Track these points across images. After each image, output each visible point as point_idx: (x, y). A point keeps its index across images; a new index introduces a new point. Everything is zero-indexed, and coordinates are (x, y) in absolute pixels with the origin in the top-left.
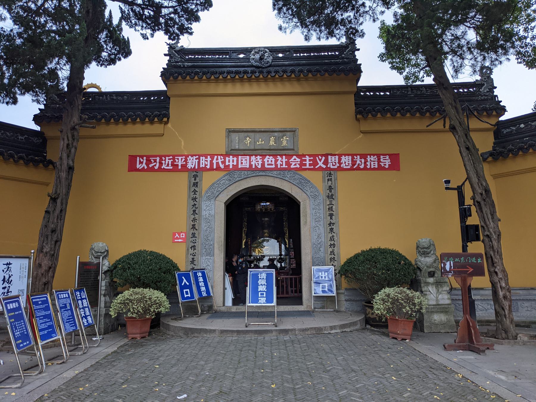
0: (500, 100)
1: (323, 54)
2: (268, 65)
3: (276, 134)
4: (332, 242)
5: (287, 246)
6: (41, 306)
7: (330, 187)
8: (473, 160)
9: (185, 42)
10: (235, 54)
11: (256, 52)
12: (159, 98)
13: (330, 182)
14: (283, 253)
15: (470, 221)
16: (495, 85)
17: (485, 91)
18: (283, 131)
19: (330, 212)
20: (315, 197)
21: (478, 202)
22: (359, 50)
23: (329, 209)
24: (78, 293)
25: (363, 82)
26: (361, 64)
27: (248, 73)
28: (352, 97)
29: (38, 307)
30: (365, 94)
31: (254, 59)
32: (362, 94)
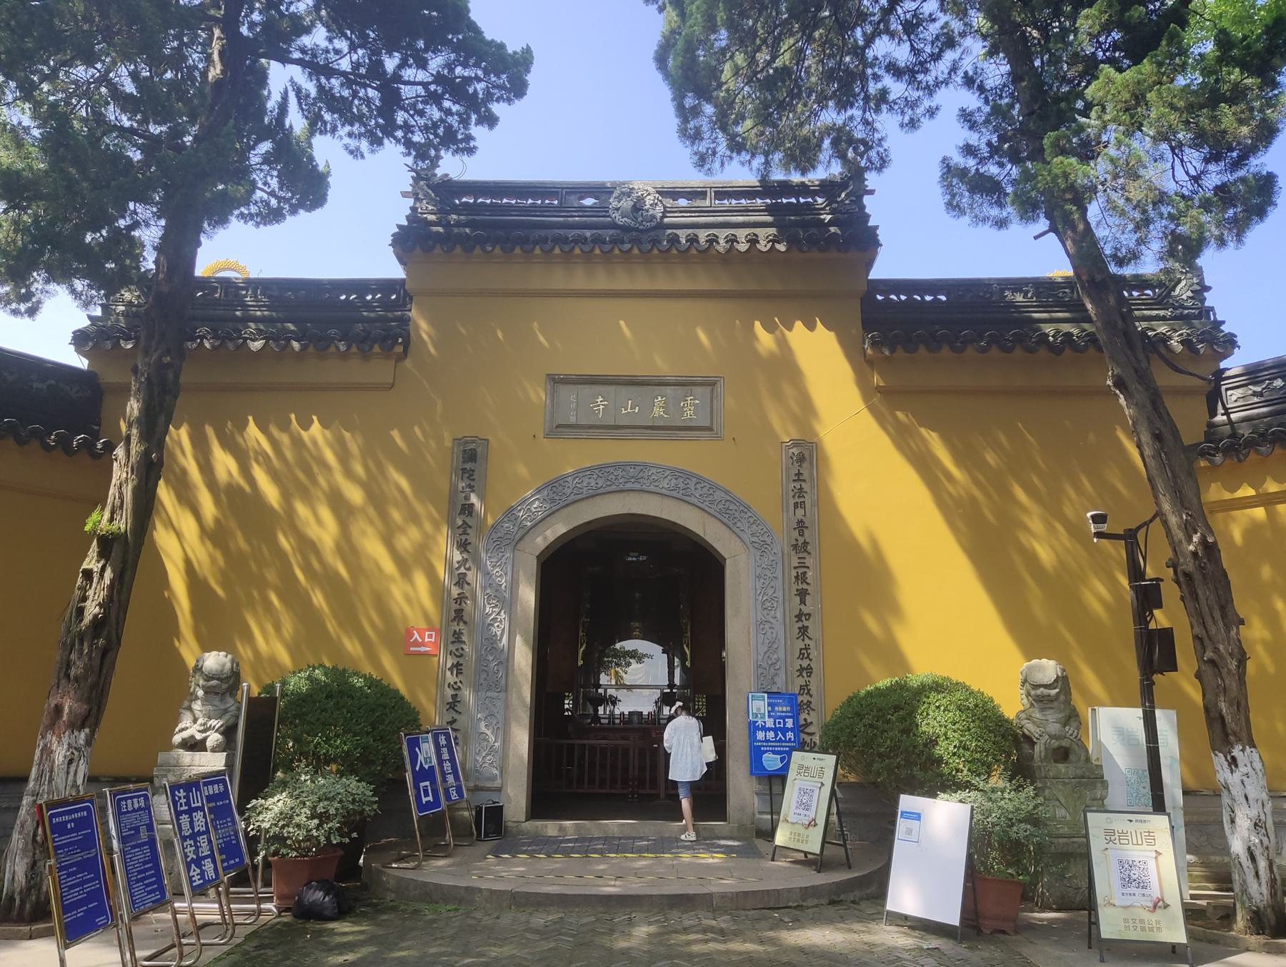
0: (1219, 318)
1: (785, 201)
2: (653, 224)
3: (669, 390)
4: (805, 663)
5: (688, 664)
6: (74, 837)
7: (800, 522)
8: (1170, 467)
9: (451, 166)
10: (572, 198)
11: (623, 193)
12: (386, 295)
13: (800, 512)
14: (677, 681)
15: (1160, 619)
16: (1207, 283)
17: (1184, 297)
18: (686, 384)
19: (800, 586)
20: (763, 548)
21: (1186, 575)
22: (872, 192)
23: (797, 577)
24: (182, 794)
25: (879, 271)
26: (877, 227)
27: (604, 242)
28: (857, 305)
29: (65, 839)
30: (887, 300)
31: (617, 209)
32: (879, 297)
